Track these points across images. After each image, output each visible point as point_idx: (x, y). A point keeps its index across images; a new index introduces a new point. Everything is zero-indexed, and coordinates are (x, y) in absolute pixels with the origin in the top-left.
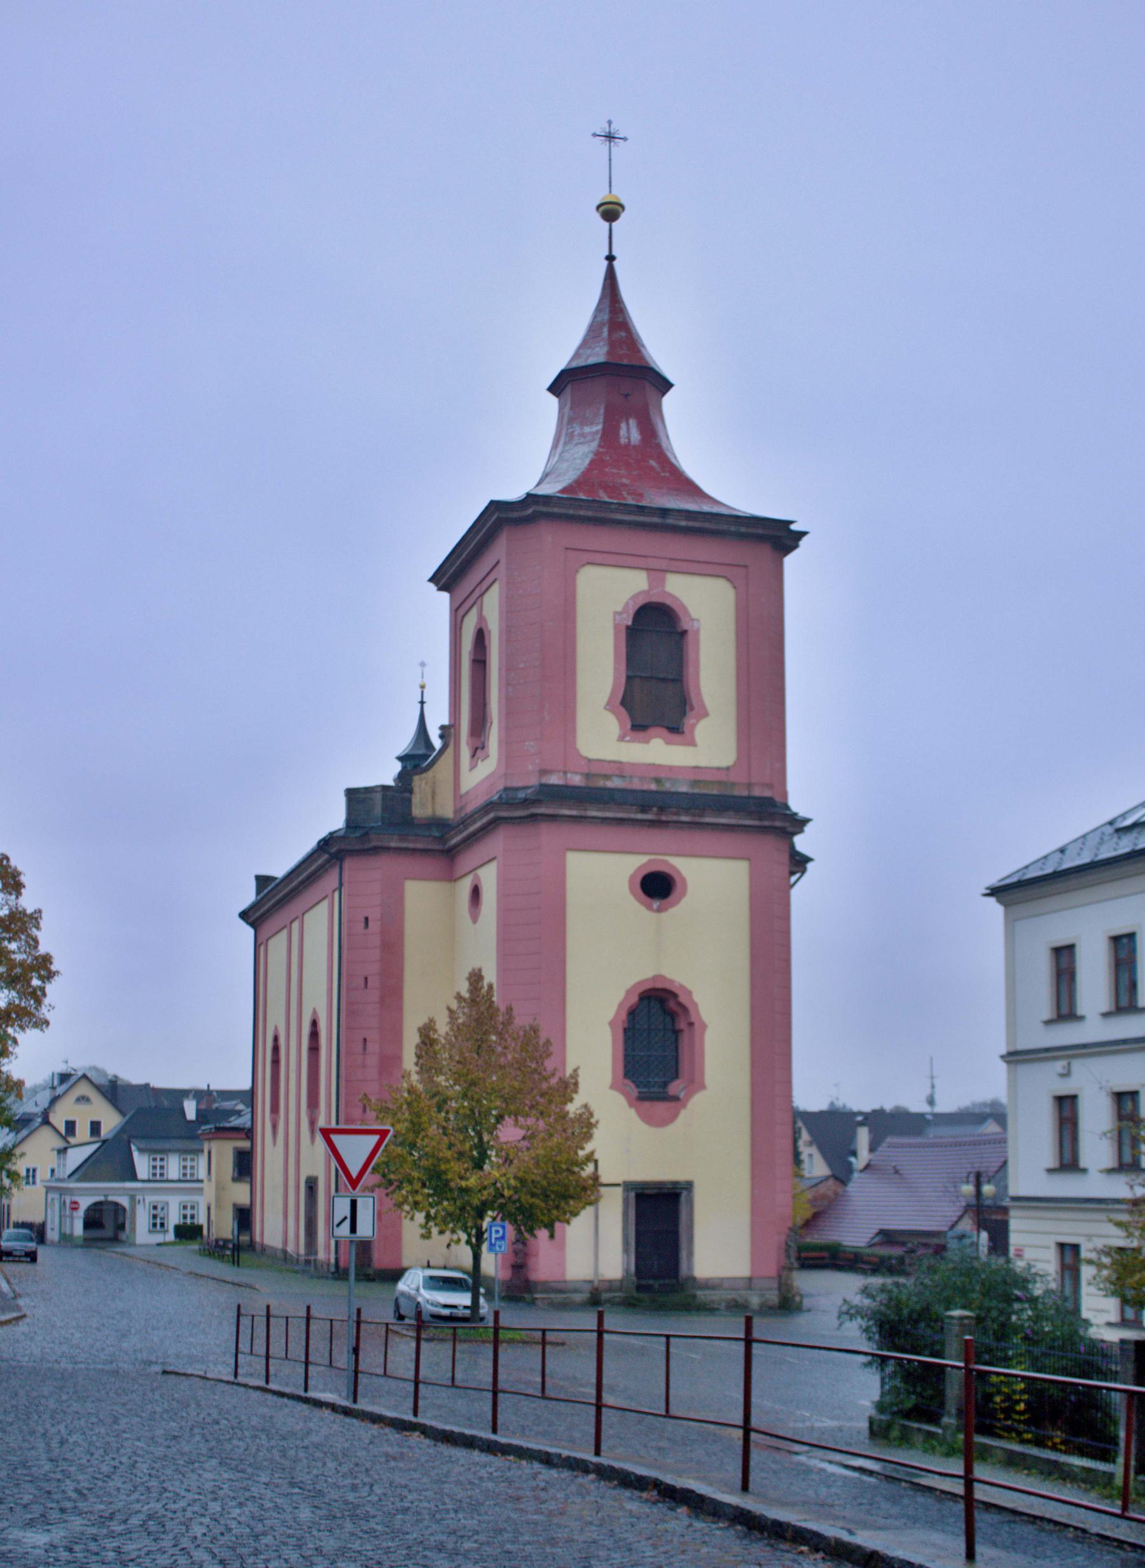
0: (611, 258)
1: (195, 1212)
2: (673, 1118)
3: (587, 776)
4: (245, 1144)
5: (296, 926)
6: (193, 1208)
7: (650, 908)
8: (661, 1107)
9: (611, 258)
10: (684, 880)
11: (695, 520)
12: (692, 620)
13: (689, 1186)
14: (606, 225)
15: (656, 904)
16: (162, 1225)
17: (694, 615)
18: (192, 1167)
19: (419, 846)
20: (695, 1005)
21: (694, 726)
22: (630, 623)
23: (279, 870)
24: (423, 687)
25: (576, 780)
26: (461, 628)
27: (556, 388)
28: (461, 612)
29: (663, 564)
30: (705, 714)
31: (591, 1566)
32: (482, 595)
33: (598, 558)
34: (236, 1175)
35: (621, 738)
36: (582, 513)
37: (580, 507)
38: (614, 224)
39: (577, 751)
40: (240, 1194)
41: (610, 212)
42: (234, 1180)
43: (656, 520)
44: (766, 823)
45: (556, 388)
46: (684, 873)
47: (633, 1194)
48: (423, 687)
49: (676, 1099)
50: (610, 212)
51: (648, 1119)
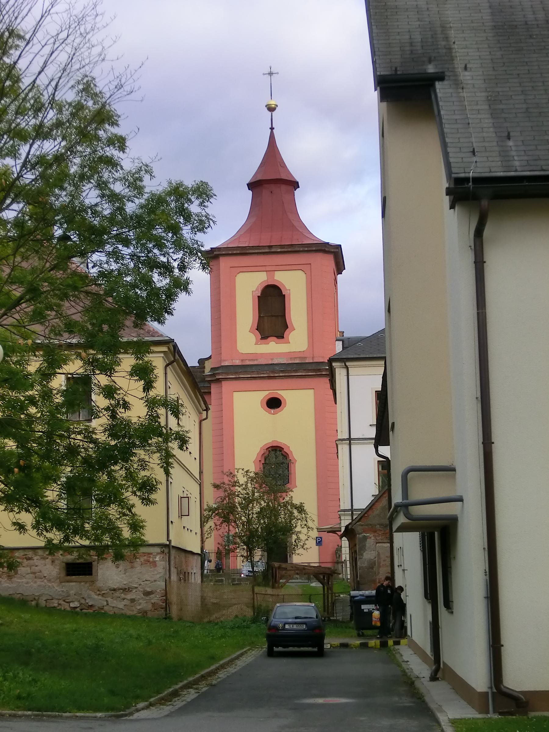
0: (272, 128)
3: (242, 360)
7: (270, 413)
9: (272, 128)
10: (285, 400)
11: (284, 248)
14: (270, 113)
15: (272, 411)
22: (259, 295)
25: (237, 362)
27: (252, 186)
29: (273, 268)
31: (3, 567)
33: (244, 269)
35: (256, 344)
36: (235, 252)
37: (234, 250)
38: (274, 113)
41: (271, 109)
43: (267, 250)
44: (319, 373)
45: (252, 186)
50: (271, 109)
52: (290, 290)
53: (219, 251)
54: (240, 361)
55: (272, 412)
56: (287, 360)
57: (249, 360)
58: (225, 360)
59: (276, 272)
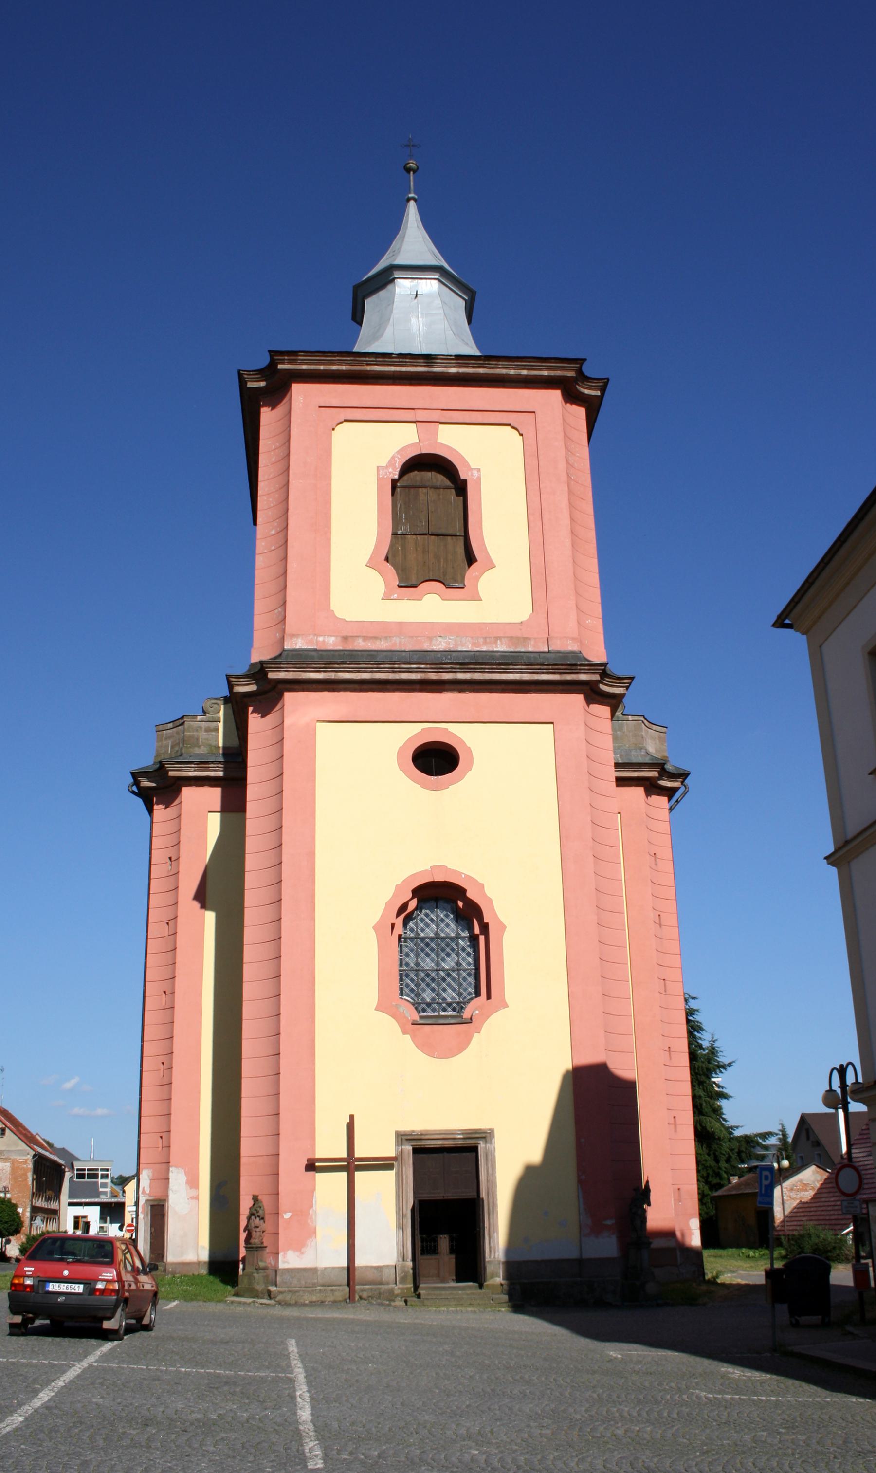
2: (462, 1046)
3: (345, 638)
13: (486, 1135)
25: (331, 642)
47: (408, 1148)
49: (469, 1022)
52: (479, 470)
53: (291, 362)
54: (339, 639)
56: (473, 644)
57: (365, 638)
58: (293, 636)
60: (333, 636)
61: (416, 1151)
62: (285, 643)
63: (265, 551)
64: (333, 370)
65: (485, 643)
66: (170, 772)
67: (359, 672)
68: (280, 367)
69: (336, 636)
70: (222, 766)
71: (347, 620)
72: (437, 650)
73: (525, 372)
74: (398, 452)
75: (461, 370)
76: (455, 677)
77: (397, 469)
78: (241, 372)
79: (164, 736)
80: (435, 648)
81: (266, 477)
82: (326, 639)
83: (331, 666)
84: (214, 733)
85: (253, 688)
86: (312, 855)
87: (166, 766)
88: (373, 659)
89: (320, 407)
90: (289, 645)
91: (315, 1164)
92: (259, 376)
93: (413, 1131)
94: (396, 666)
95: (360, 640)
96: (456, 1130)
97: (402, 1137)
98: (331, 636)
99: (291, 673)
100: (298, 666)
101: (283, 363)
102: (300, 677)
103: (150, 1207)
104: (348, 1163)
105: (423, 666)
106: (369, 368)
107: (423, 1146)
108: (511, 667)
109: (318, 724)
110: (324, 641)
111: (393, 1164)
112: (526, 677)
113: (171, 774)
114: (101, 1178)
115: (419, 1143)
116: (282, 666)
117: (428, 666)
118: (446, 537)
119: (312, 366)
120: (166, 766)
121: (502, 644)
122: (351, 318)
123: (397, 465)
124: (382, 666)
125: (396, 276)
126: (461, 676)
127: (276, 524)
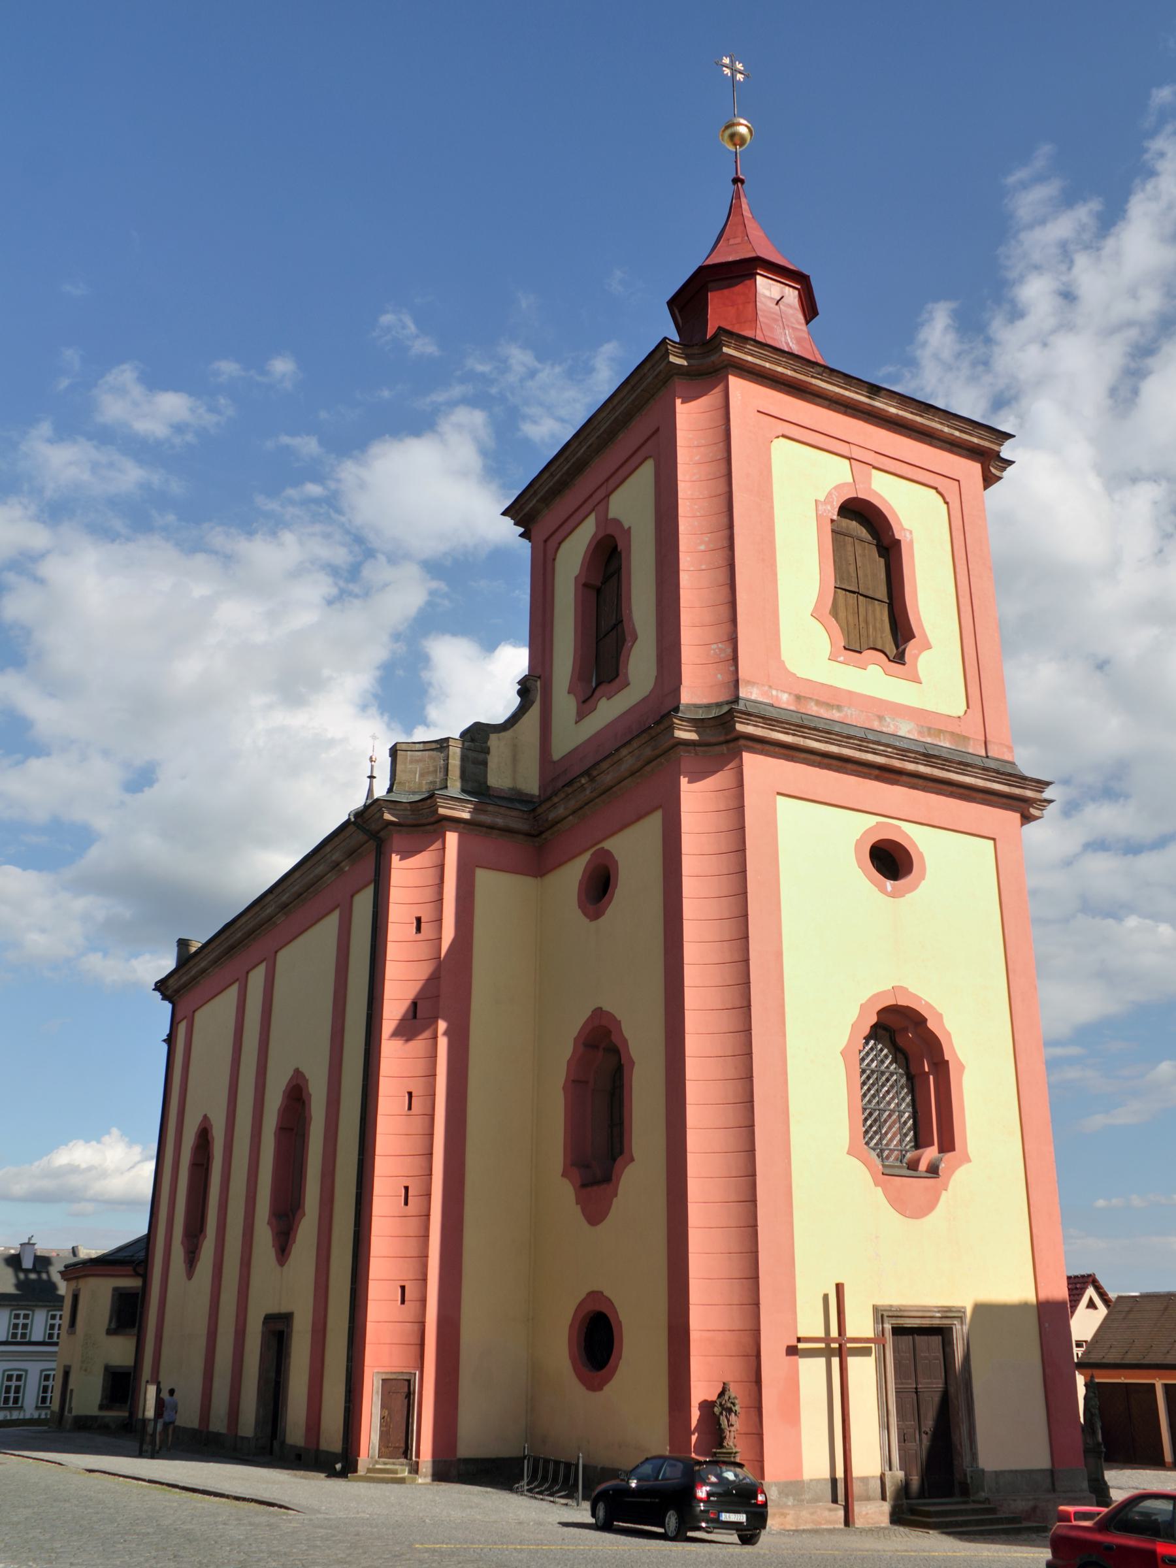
1: (6, 1383)
2: (930, 1206)
3: (798, 698)
4: (131, 1283)
5: (257, 978)
6: (19, 1378)
7: (883, 890)
8: (918, 1186)
12: (904, 529)
16: (16, 1400)
17: (906, 525)
18: (25, 1326)
19: (500, 821)
20: (949, 1034)
21: (916, 657)
23: (161, 997)
24: (371, 777)
25: (784, 700)
26: (554, 560)
28: (552, 544)
30: (927, 646)
32: (608, 496)
34: (113, 1326)
38: (734, 175)
39: (782, 664)
40: (119, 1351)
42: (110, 1332)
46: (922, 847)
48: (371, 777)
51: (900, 1205)
52: (911, 532)
54: (792, 697)
55: (889, 888)
56: (920, 733)
57: (818, 703)
58: (749, 683)
59: (874, 472)
60: (786, 692)
61: (898, 1331)
62: (741, 689)
63: (692, 569)
64: (778, 372)
65: (930, 735)
66: (439, 809)
67: (826, 742)
68: (725, 350)
69: (790, 694)
70: (472, 806)
71: (798, 675)
72: (886, 732)
73: (957, 433)
74: (835, 488)
75: (901, 413)
76: (917, 769)
77: (835, 508)
78: (667, 341)
79: (409, 758)
80: (885, 730)
81: (687, 478)
82: (780, 694)
83: (802, 729)
84: (481, 767)
85: (693, 736)
86: (779, 955)
87: (438, 800)
88: (826, 732)
89: (758, 411)
90: (745, 693)
91: (1076, 1363)
92: (680, 351)
93: (891, 1306)
94: (865, 744)
95: (813, 704)
96: (931, 1307)
97: (880, 1314)
98: (784, 692)
99: (760, 729)
100: (768, 722)
101: (728, 347)
102: (769, 736)
103: (381, 1382)
104: (840, 1345)
105: (889, 750)
106: (814, 381)
107: (901, 1326)
108: (969, 769)
109: (780, 799)
110: (777, 696)
111: (871, 1348)
112: (980, 783)
113: (441, 811)
114: (24, 1319)
115: (900, 1321)
116: (752, 718)
117: (895, 751)
118: (873, 601)
119: (758, 360)
120: (438, 800)
121: (944, 739)
122: (667, 301)
123: (835, 503)
124: (852, 741)
125: (758, 271)
126: (922, 769)
127: (707, 539)
